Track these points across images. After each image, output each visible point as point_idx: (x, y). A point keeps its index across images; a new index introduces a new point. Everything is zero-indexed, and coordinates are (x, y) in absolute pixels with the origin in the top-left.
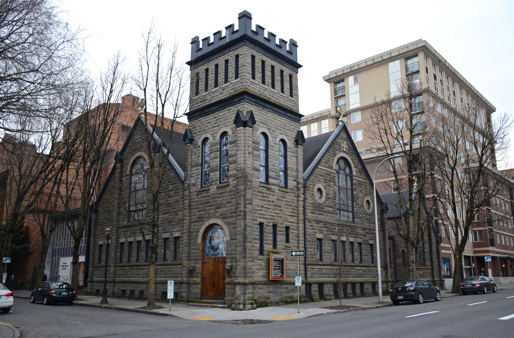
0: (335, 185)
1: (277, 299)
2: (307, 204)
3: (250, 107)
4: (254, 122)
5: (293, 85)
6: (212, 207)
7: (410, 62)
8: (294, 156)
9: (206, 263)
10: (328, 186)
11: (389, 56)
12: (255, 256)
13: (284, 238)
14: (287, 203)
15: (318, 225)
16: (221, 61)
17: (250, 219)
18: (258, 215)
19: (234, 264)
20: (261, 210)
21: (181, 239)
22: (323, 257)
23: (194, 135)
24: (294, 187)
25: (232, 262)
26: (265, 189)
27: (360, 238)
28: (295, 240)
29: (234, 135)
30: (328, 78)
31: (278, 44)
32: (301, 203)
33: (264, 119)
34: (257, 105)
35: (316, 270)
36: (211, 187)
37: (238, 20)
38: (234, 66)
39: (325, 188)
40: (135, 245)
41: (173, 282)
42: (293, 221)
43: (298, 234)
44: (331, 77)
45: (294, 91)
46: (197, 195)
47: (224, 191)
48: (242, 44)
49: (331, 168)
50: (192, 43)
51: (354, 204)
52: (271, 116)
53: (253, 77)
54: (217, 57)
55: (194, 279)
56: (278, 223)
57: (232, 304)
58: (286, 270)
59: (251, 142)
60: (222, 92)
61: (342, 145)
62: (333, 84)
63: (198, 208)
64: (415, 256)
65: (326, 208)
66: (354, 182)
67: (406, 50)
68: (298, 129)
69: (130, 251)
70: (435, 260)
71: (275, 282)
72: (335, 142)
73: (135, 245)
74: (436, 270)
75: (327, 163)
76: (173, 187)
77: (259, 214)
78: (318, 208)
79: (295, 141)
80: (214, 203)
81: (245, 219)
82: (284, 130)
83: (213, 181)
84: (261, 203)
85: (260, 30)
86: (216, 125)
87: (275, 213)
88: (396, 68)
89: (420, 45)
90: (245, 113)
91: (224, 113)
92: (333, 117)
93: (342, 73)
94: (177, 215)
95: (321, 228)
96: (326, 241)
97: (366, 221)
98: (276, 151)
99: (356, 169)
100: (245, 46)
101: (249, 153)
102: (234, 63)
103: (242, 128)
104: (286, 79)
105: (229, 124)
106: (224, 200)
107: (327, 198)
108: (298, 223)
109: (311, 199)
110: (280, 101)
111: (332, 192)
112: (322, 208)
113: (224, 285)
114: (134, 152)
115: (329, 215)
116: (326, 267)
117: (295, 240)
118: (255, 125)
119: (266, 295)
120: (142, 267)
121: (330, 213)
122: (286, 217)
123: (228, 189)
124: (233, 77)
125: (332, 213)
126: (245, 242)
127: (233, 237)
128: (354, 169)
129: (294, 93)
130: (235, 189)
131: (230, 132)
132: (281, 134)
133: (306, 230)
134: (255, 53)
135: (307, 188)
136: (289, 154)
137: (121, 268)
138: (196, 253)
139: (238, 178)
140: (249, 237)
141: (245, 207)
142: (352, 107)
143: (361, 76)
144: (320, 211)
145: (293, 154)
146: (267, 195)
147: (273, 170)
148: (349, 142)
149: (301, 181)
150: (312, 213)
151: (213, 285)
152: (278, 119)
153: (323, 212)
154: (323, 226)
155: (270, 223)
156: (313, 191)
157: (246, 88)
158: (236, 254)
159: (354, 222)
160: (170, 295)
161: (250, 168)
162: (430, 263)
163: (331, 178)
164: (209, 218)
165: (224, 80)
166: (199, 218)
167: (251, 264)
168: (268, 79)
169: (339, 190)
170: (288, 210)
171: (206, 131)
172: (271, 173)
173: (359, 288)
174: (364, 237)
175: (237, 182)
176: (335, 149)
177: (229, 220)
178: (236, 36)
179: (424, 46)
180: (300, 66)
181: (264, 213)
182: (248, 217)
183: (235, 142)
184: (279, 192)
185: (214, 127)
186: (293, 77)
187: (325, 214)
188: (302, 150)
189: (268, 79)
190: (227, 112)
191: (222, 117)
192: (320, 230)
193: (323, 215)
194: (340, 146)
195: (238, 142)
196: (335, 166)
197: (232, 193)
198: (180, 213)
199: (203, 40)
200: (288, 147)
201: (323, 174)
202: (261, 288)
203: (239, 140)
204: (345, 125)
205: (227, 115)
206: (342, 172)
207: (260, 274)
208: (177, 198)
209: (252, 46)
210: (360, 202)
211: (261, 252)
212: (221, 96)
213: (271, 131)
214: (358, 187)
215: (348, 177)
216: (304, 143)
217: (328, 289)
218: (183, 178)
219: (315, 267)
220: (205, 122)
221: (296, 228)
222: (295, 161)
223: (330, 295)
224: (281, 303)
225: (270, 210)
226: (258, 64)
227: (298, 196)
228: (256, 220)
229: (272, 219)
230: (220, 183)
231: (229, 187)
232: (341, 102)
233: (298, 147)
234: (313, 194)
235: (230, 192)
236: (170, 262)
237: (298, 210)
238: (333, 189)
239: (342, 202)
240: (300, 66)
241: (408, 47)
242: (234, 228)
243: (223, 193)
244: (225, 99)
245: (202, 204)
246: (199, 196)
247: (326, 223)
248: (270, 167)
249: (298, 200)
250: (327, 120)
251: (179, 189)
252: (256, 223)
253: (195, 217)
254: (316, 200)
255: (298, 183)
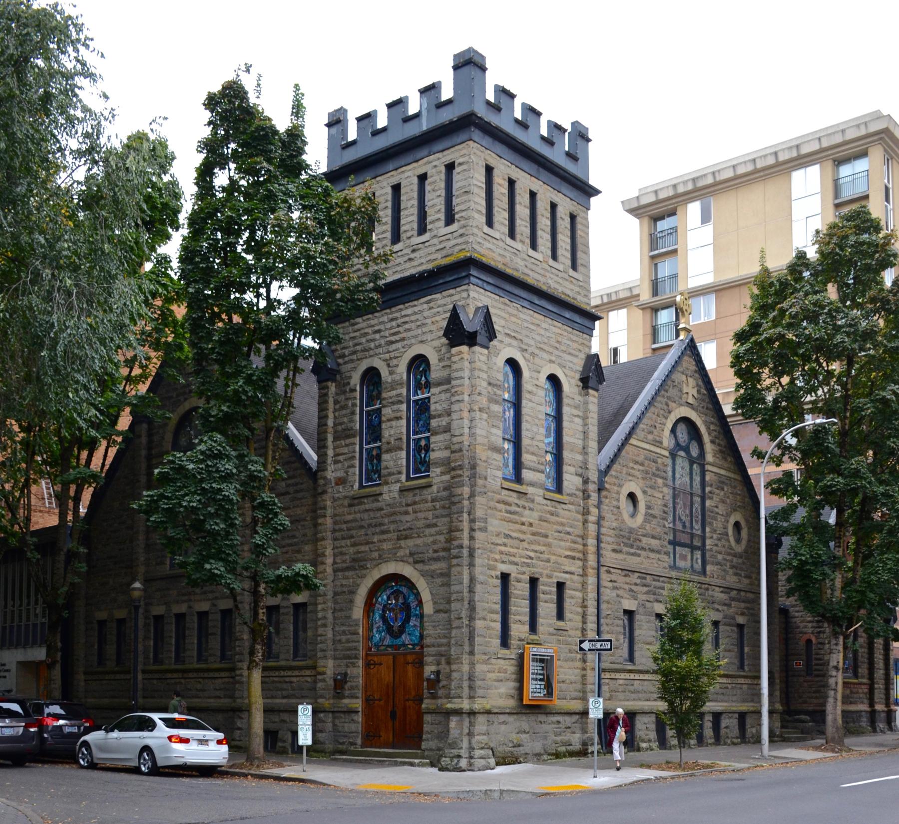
0: (666, 485)
1: (538, 747)
2: (603, 530)
3: (482, 298)
4: (492, 334)
5: (579, 240)
6: (389, 536)
7: (845, 171)
8: (578, 416)
9: (375, 664)
10: (651, 487)
11: (794, 154)
12: (491, 650)
13: (553, 608)
14: (560, 528)
15: (627, 579)
16: (407, 176)
17: (483, 566)
18: (497, 557)
19: (444, 668)
20: (505, 545)
21: (309, 608)
22: (637, 655)
23: (340, 361)
24: (578, 489)
25: (438, 664)
26: (514, 495)
27: (718, 610)
28: (578, 613)
29: (441, 364)
30: (635, 205)
31: (492, 100)
32: (592, 528)
33: (513, 327)
34: (497, 291)
35: (621, 682)
36: (385, 489)
37: (452, 71)
38: (443, 193)
39: (645, 492)
40: (193, 623)
41: (310, 707)
42: (573, 569)
43: (584, 600)
44: (645, 201)
45: (580, 254)
46: (350, 505)
47: (417, 499)
48: (463, 136)
49: (658, 443)
50: (329, 125)
51: (708, 530)
52: (528, 318)
53: (490, 223)
54: (396, 166)
55: (346, 701)
56: (541, 574)
57: (441, 756)
58: (559, 682)
59: (485, 384)
60: (412, 256)
61: (685, 390)
62: (646, 220)
63: (352, 537)
64: (841, 655)
65: (644, 540)
66: (708, 478)
67: (838, 139)
68: (587, 350)
69: (181, 636)
70: (879, 663)
71: (535, 709)
72: (669, 382)
73: (193, 623)
74: (880, 686)
75: (651, 432)
76: (288, 486)
77: (501, 553)
78: (629, 540)
79: (582, 380)
80: (392, 527)
81: (471, 565)
82: (557, 353)
83: (390, 474)
84: (505, 528)
85: (504, 99)
86: (397, 337)
87: (536, 551)
88: (808, 182)
89: (874, 127)
90: (471, 311)
91: (416, 309)
92: (643, 308)
93: (671, 193)
94: (299, 552)
95: (634, 588)
96: (642, 617)
97: (731, 571)
98: (538, 403)
99: (713, 447)
100: (471, 143)
101: (481, 410)
102: (443, 185)
103: (464, 348)
104: (564, 224)
105: (429, 337)
106: (417, 519)
107: (649, 517)
108: (584, 575)
109: (613, 517)
110: (550, 281)
111: (660, 502)
112: (636, 540)
113: (420, 715)
114: (182, 398)
115: (652, 555)
116: (642, 677)
117: (578, 613)
118: (494, 342)
119: (514, 737)
120: (211, 675)
121: (652, 551)
122: (557, 562)
123: (428, 494)
124: (439, 219)
125: (658, 552)
126: (471, 619)
127: (441, 607)
128: (709, 447)
129: (579, 262)
130: (445, 494)
131: (433, 358)
132: (551, 361)
133: (602, 590)
134: (494, 161)
135: (604, 493)
136: (566, 410)
137: (157, 676)
138: (348, 641)
139: (454, 469)
140: (479, 606)
141: (472, 538)
142: (694, 282)
143: (721, 205)
144: (632, 546)
145: (576, 412)
146: (518, 509)
147: (532, 449)
148: (701, 383)
149: (594, 476)
150: (614, 551)
151: (393, 715)
152: (544, 325)
153: (638, 548)
154: (638, 581)
155: (524, 573)
156: (618, 500)
157: (474, 250)
158: (448, 645)
159: (704, 572)
160: (305, 737)
161: (484, 445)
162: (866, 671)
163: (658, 469)
164: (382, 559)
165: (415, 226)
166: (354, 560)
167: (485, 667)
168: (522, 226)
169: (675, 497)
170: (562, 543)
171: (372, 353)
172: (526, 458)
173: (710, 724)
174: (725, 608)
175: (453, 478)
176: (669, 398)
177: (432, 568)
178: (447, 116)
179: (886, 131)
180: (596, 192)
181: (512, 550)
182: (478, 561)
183: (448, 380)
184: (545, 502)
185: (392, 342)
186: (579, 219)
187: (643, 553)
188: (596, 400)
189: (522, 226)
190: (425, 306)
191: (413, 318)
192: (631, 590)
193: (639, 555)
194: (681, 391)
195: (453, 383)
196: (667, 440)
197: (438, 505)
198: (307, 548)
199: (360, 119)
200: (564, 395)
201: (641, 459)
202: (505, 723)
203: (457, 378)
204: (692, 340)
205: (426, 314)
206: (682, 453)
207: (503, 690)
208: (299, 512)
209: (487, 141)
210: (720, 525)
211: (505, 641)
212: (408, 265)
213: (527, 356)
214: (717, 491)
215: (695, 466)
216: (491, 340)
217: (644, 727)
218: (314, 466)
219: (618, 676)
220: (369, 330)
221: (579, 586)
222: (581, 428)
223: (650, 741)
224: (545, 757)
225: (525, 545)
226: (500, 190)
227: (586, 512)
228: (493, 568)
229: (528, 565)
230: (408, 478)
231: (430, 490)
232: (665, 269)
233: (587, 394)
234: (619, 508)
235: (433, 501)
236: (283, 663)
237: (585, 545)
238: (660, 496)
239: (679, 526)
240: (596, 192)
241: (843, 131)
242: (443, 585)
243: (415, 503)
244: (421, 274)
245: (362, 527)
246: (356, 508)
247: (643, 575)
248: (525, 442)
249: (585, 522)
250: (623, 312)
251: (301, 490)
252: (493, 573)
253: (345, 558)
254: (623, 522)
255: (586, 481)
